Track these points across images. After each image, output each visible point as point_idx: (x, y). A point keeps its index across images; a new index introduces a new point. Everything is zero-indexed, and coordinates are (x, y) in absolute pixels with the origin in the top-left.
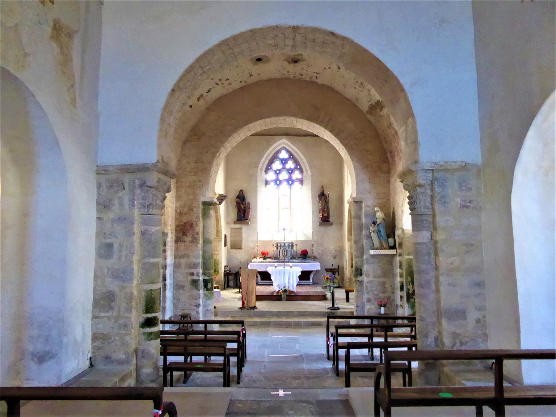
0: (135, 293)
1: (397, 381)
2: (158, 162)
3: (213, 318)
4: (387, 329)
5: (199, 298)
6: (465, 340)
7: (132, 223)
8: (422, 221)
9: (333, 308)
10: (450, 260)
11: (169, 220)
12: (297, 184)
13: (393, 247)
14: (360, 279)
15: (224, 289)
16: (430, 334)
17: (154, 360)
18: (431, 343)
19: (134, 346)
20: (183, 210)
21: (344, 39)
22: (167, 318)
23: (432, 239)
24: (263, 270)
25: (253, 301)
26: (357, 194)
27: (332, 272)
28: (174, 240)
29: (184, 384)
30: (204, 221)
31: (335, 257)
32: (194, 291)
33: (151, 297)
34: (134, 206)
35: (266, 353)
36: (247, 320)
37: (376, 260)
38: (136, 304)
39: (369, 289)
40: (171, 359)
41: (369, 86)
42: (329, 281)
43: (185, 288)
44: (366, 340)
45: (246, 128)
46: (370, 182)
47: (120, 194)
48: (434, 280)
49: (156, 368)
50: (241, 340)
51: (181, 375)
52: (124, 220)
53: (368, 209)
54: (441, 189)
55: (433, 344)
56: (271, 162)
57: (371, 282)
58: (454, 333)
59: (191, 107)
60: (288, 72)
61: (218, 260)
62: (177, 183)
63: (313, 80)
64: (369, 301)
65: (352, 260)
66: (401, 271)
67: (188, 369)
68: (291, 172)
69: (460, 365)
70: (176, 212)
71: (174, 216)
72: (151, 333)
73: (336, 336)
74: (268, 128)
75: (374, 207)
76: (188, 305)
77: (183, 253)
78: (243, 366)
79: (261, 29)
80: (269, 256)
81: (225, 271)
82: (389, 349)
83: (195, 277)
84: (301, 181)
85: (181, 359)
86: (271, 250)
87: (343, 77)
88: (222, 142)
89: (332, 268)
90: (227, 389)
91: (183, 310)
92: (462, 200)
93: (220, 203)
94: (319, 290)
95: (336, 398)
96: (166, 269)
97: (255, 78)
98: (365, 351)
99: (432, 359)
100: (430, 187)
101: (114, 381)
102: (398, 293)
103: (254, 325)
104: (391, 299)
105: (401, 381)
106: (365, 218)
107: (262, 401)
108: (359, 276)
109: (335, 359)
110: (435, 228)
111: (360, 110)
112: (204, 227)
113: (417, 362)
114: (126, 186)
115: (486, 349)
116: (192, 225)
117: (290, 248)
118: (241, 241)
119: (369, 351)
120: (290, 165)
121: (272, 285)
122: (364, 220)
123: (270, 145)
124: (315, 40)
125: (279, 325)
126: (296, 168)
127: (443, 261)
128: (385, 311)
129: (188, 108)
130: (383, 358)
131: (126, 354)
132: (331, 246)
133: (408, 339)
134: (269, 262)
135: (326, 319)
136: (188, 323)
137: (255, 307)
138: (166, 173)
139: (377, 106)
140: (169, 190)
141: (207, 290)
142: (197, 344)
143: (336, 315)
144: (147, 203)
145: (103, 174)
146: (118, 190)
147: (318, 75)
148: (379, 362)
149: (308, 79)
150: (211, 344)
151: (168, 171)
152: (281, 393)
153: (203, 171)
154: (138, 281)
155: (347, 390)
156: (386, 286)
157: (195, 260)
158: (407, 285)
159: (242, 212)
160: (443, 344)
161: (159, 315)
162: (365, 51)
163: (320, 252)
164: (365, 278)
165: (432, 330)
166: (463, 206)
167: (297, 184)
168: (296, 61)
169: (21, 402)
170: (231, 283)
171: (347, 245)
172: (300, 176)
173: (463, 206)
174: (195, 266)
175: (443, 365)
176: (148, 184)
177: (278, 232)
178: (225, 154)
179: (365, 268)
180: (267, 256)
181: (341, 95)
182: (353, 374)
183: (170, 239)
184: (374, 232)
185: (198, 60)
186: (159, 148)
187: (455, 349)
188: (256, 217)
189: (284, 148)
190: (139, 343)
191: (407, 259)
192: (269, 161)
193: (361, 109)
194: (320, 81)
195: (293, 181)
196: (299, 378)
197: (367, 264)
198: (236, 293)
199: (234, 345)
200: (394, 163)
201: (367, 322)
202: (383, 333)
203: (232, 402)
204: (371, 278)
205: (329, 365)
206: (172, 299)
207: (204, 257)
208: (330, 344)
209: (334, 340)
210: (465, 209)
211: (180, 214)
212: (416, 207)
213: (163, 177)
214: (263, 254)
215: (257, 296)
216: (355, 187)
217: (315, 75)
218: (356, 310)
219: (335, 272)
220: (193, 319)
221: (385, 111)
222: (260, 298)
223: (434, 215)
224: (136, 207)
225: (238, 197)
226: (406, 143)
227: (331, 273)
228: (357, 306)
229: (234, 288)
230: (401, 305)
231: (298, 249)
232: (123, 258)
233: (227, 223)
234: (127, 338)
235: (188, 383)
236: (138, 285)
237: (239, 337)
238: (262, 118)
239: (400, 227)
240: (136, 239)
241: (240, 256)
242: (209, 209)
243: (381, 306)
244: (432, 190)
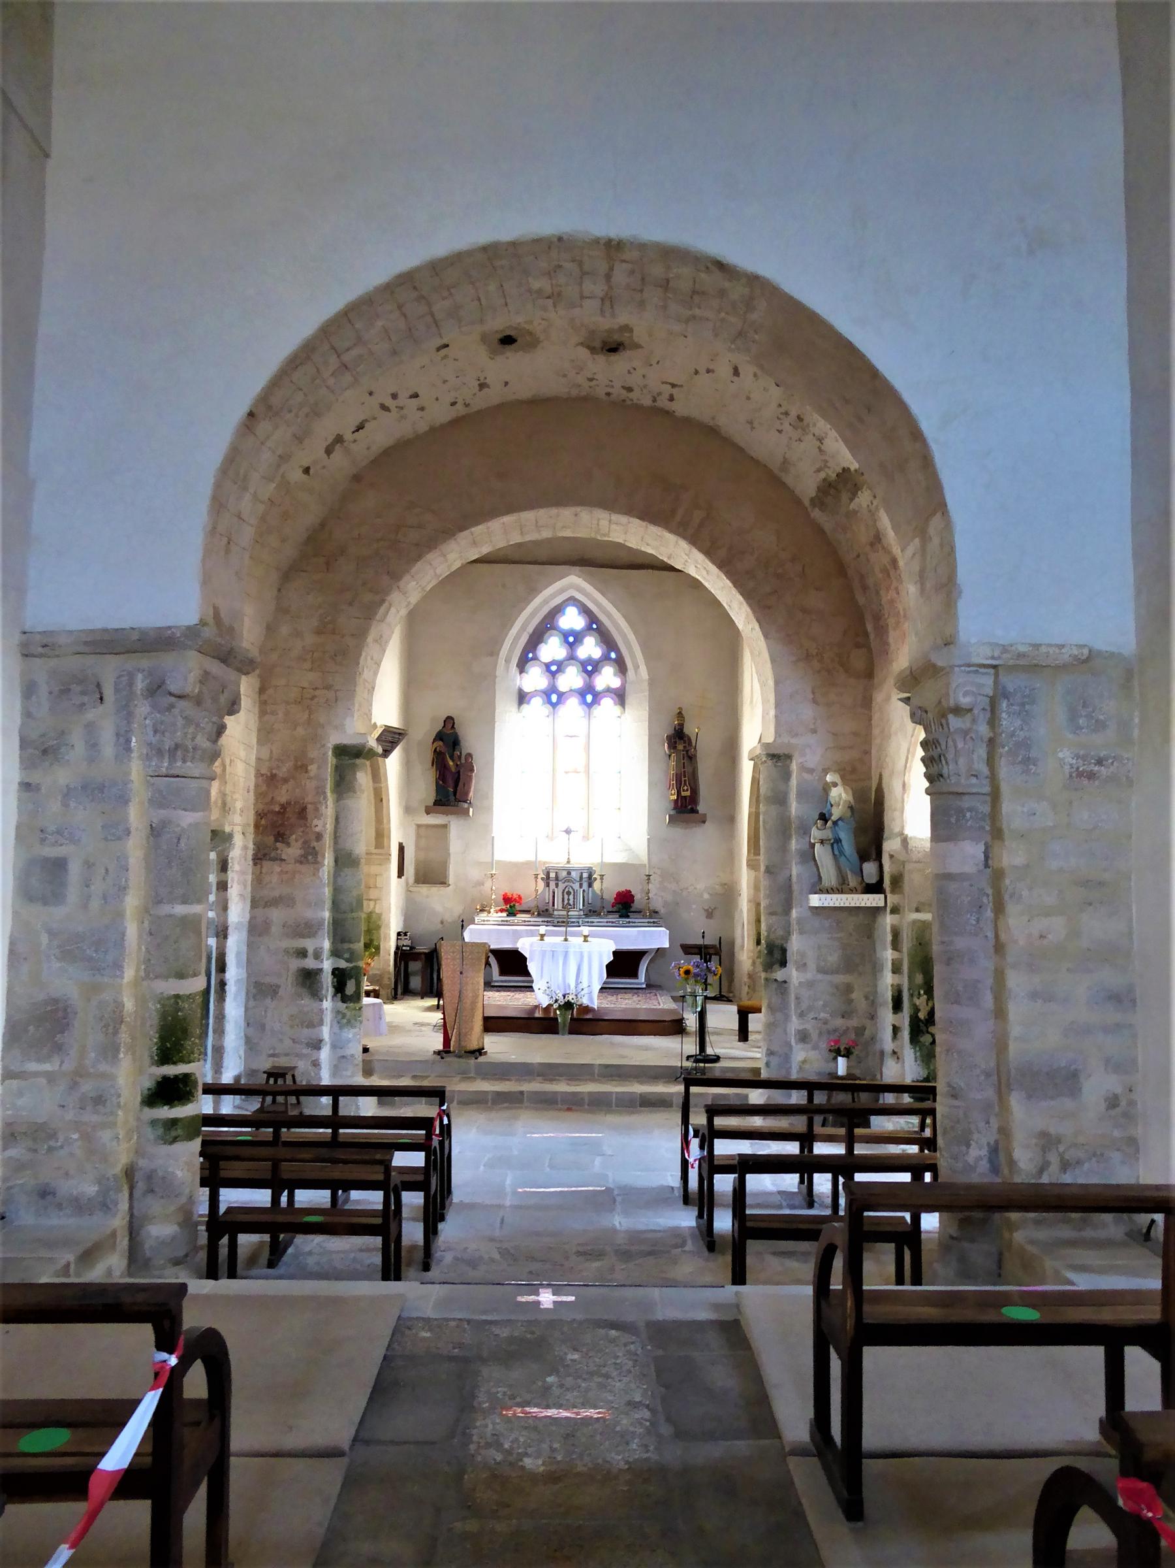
0: (129, 1005)
1: (879, 1271)
2: (203, 623)
3: (360, 1080)
4: (853, 1120)
5: (321, 1023)
6: (1071, 1155)
7: (123, 800)
8: (961, 812)
9: (703, 1057)
10: (1040, 924)
11: (236, 796)
12: (607, 703)
13: (875, 888)
14: (780, 975)
15: (395, 997)
16: (976, 1136)
17: (183, 1200)
18: (980, 1158)
19: (123, 1159)
20: (278, 767)
21: (754, 280)
22: (227, 1078)
23: (987, 866)
24: (507, 945)
25: (475, 1035)
26: (778, 733)
27: (700, 953)
28: (250, 853)
29: (270, 1271)
31: (710, 914)
32: (307, 1002)
33: (175, 1018)
34: (128, 749)
35: (508, 1182)
36: (456, 1086)
37: (827, 923)
38: (133, 1038)
39: (804, 1006)
40: (231, 1197)
41: (821, 425)
42: (692, 981)
43: (281, 992)
44: (792, 1148)
45: (464, 537)
46: (815, 701)
47: (91, 715)
48: (990, 981)
49: (187, 1221)
50: (435, 1142)
51: (262, 1243)
52: (104, 793)
53: (806, 776)
54: (1018, 723)
55: (984, 1165)
57: (810, 984)
58: (1044, 1135)
59: (307, 471)
60: (591, 380)
61: (379, 916)
62: (262, 690)
63: (659, 404)
64: (803, 1037)
65: (758, 921)
66: (896, 955)
67: (281, 1227)
68: (591, 668)
69: (1058, 1228)
70: (259, 774)
71: (252, 787)
72: (173, 1123)
73: (709, 1136)
74: (528, 538)
75: (826, 771)
76: (288, 1042)
77: (276, 894)
78: (442, 1218)
79: (514, 244)
80: (524, 907)
81: (397, 948)
82: (859, 1177)
83: (310, 963)
84: (620, 696)
85: (261, 1197)
86: (530, 890)
87: (748, 398)
88: (396, 576)
89: (700, 942)
90: (392, 1287)
91: (273, 1055)
92: (1078, 757)
93: (387, 753)
94: (663, 1004)
95: (703, 1315)
96: (225, 937)
97: (494, 396)
98: (790, 1181)
99: (981, 1208)
100: (988, 715)
101: (63, 1262)
102: (887, 1017)
103: (478, 1101)
104: (867, 1033)
105: (892, 1269)
106: (798, 802)
107: (491, 1322)
108: (776, 966)
109: (704, 1201)
110: (997, 834)
111: (792, 492)
112: (337, 819)
113: (937, 1214)
114: (109, 692)
115: (1133, 1181)
116: (302, 813)
117: (585, 886)
119: (802, 1181)
120: (590, 648)
121: (530, 988)
122: (794, 807)
123: (533, 591)
124: (668, 281)
125: (547, 1103)
126: (606, 658)
127: (1019, 926)
128: (848, 1067)
129: (296, 475)
130: (842, 1201)
131: (99, 1183)
132: (699, 883)
133: (914, 1149)
134: (525, 923)
135: (680, 1088)
136: (287, 1093)
137: (480, 1052)
138: (227, 656)
139: (841, 485)
140: (233, 708)
141: (344, 999)
142: (306, 1154)
143: (708, 1075)
144: (168, 744)
145: (41, 656)
146: (84, 704)
147: (675, 391)
148: (828, 1212)
149: (647, 402)
150: (350, 1156)
151: (231, 651)
152: (546, 1298)
153: (336, 661)
154: (137, 970)
155: (737, 1293)
156: (854, 996)
157: (309, 914)
158: (912, 995)
159: (451, 782)
160: (1012, 1163)
161: (203, 1071)
162: (813, 319)
163: (669, 898)
164: (793, 974)
165: (982, 1125)
166: (1080, 775)
167: (607, 703)
168: (613, 348)
170: (416, 982)
171: (745, 879)
172: (616, 683)
173: (1080, 775)
174: (308, 929)
175: (1012, 1227)
176: (173, 688)
177: (551, 838)
178: (404, 612)
179: (795, 945)
180: (518, 907)
181: (741, 450)
182: (753, 1247)
183: (240, 850)
184: (822, 842)
185: (327, 331)
186: (206, 580)
187: (1045, 1179)
188: (488, 796)
189: (572, 601)
190: (139, 1152)
191: (914, 922)
192: (531, 636)
193: (797, 492)
194: (680, 408)
195: (597, 697)
196: (599, 1255)
198: (429, 1009)
199: (417, 1159)
200: (885, 650)
201: (797, 1098)
202: (842, 1131)
203: (402, 1326)
204: (809, 975)
205: (687, 1219)
206: (242, 1023)
207: (336, 906)
208: (691, 1160)
209: (702, 1147)
210: (1085, 782)
211: (268, 780)
212: (945, 772)
213: (216, 668)
214: (507, 899)
215: (486, 1019)
216: (772, 713)
217: (667, 389)
218: (768, 1064)
219: (709, 954)
220: (302, 1081)
221: (864, 498)
222: (494, 1024)
223: (995, 796)
224: (134, 755)
225: (440, 737)
226: (922, 590)
227: (697, 958)
228: (770, 1053)
229: (423, 995)
230: (894, 1053)
231: (607, 888)
232: (95, 904)
233: (408, 810)
234: (105, 1136)
235: (281, 1269)
236: (136, 983)
237: (429, 1136)
238: (510, 509)
239: (897, 830)
240: (135, 849)
241: (441, 903)
242: (354, 768)
243: (838, 1053)
244: (993, 722)
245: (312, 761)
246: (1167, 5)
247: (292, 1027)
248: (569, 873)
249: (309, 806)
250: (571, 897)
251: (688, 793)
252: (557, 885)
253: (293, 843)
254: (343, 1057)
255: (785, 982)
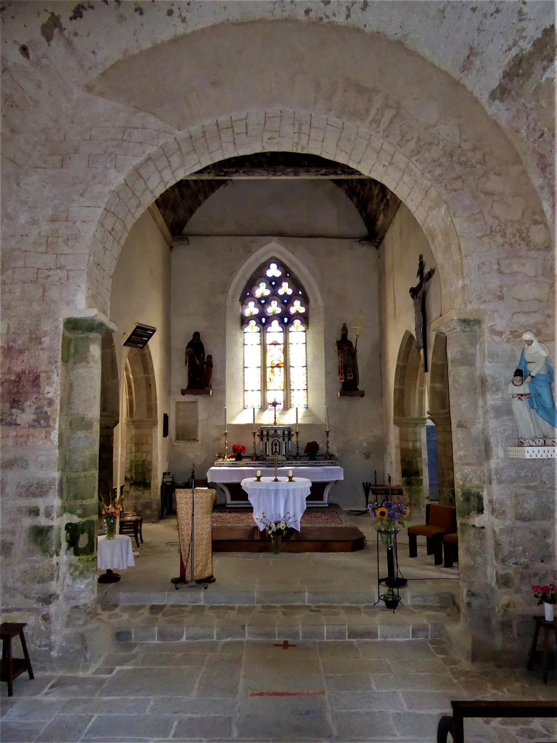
20: (14, 341)
30: (67, 372)
32: (41, 561)
56: (252, 284)
57: (510, 531)
61: (150, 463)
81: (164, 484)
83: (42, 521)
84: (305, 319)
86: (250, 443)
108: (473, 513)
116: (36, 381)
118: (196, 427)
120: (285, 289)
123: (249, 252)
132: (362, 437)
134: (247, 465)
141: (77, 553)
157: (41, 474)
169: (177, 490)
197: (500, 482)
231: (304, 439)
233: (168, 392)
241: (193, 453)
245: (46, 334)
246: (553, 3)
247: (24, 582)
248: (276, 431)
249: (42, 375)
250: (278, 447)
251: (352, 378)
252: (268, 440)
253: (27, 410)
254: (76, 607)
255: (483, 528)
